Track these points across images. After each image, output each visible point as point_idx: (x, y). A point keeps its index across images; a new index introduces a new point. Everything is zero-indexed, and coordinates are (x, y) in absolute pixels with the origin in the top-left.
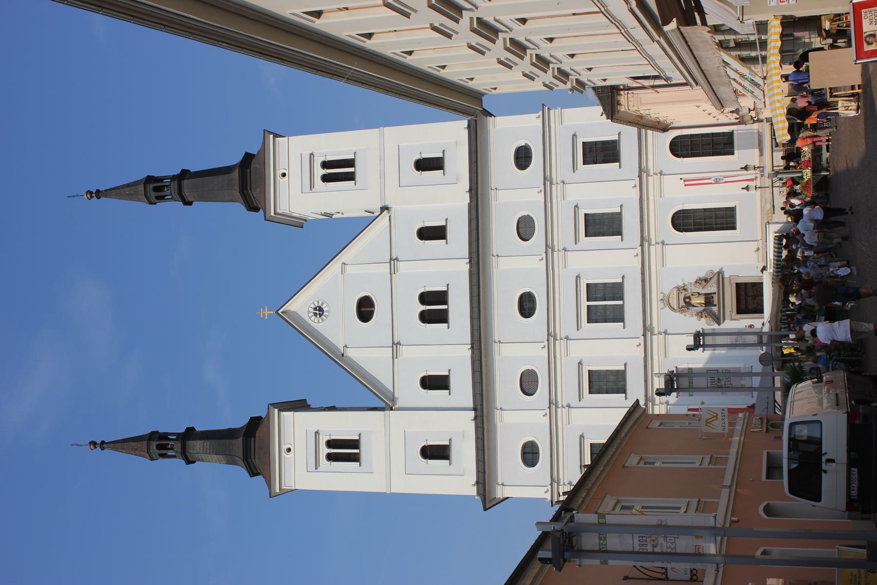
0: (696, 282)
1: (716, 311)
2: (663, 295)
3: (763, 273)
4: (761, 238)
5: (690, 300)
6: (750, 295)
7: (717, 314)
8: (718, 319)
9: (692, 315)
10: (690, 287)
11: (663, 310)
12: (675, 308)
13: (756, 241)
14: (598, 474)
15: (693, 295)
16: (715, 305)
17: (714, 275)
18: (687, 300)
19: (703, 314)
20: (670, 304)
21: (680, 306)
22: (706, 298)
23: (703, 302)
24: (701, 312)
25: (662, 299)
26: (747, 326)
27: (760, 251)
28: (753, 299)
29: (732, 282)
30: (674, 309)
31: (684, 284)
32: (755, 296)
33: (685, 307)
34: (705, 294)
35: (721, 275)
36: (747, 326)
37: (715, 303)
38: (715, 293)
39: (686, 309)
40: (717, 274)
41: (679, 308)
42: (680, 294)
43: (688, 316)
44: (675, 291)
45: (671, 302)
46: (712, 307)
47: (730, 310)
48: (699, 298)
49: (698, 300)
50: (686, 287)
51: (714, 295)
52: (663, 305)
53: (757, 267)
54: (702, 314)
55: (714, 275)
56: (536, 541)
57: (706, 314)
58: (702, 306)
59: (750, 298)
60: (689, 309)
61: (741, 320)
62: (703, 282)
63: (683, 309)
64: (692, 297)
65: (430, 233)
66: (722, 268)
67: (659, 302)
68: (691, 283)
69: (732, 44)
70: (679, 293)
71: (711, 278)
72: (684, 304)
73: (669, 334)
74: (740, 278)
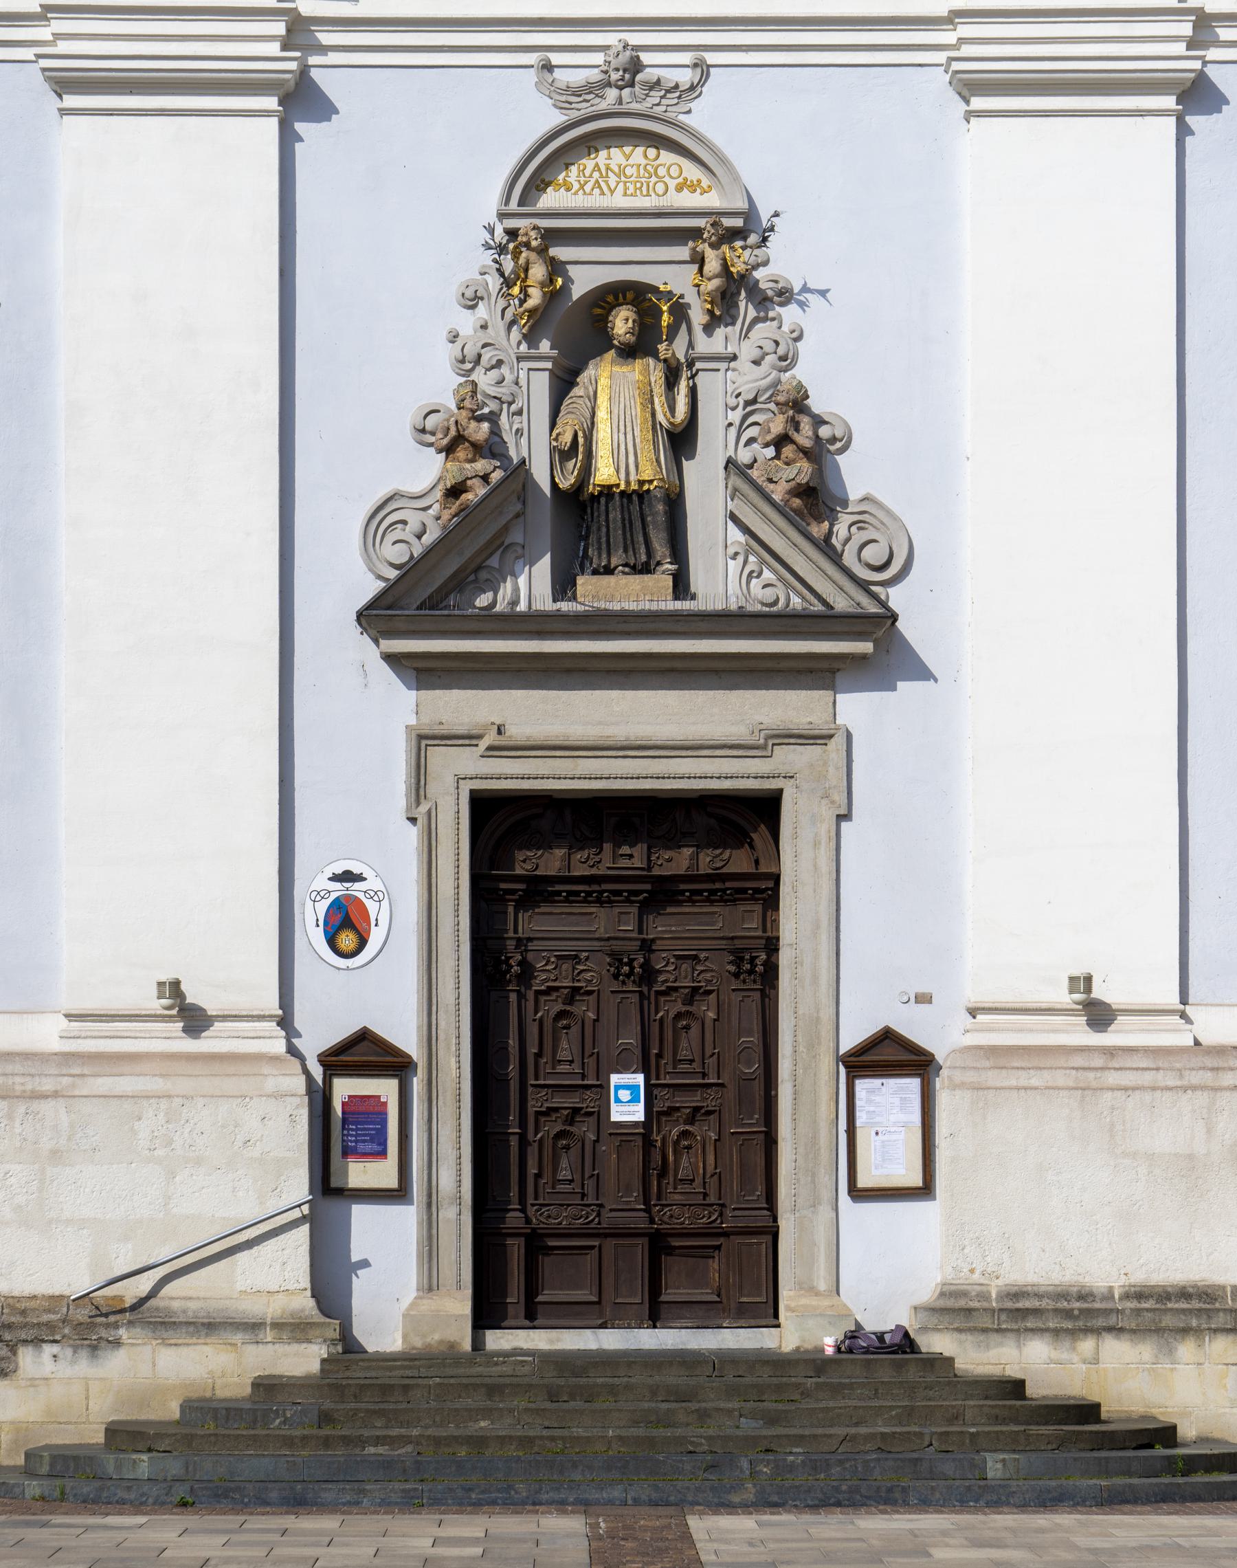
0: (797, 404)
1: (506, 590)
2: (685, 77)
3: (969, 122)
4: (1205, 1040)
5: (629, 352)
6: (661, 927)
7: (483, 600)
8: (433, 602)
9: (467, 363)
10: (747, 351)
11: (531, 76)
12: (550, 199)
13: (1184, 1000)
14: (914, 1430)
15: (671, 381)
16: (563, 586)
17: (864, 585)
18: (622, 323)
19: (481, 465)
20: (590, 143)
21: (561, 253)
22: (636, 498)
23: (604, 473)
24: (492, 448)
25: (635, 66)
26: (357, 889)
27: (1079, 1034)
28: (616, 958)
29: (789, 758)
30: (539, 183)
31: (785, 295)
32: (649, 975)
33: (554, 296)
34: (675, 503)
35: (866, 647)
36: (357, 889)
37: (585, 584)
38: (681, 586)
39: (535, 297)
40: (873, 609)
41: (552, 237)
42: (683, 252)
43: (466, 323)
44: (712, 200)
45: (615, 157)
46: (547, 559)
47: (518, 731)
48: (641, 433)
49: (619, 426)
50: (746, 309)
51: (662, 580)
52: (577, 78)
53: (923, 999)
54: (479, 450)
55: (864, 585)
56: (294, 808)
57: (478, 491)
58: (563, 455)
59: (629, 926)
60: (531, 338)
61: (412, 834)
62: (802, 471)
63: (538, 272)
64: (648, 371)
65: (883, 1084)
66: (923, 673)
67: (611, 38)
68: (787, 361)
69: (1076, 1312)
70: (696, 233)
71: (826, 547)
72: (583, 281)
73: (288, 140)
74: (829, 823)
